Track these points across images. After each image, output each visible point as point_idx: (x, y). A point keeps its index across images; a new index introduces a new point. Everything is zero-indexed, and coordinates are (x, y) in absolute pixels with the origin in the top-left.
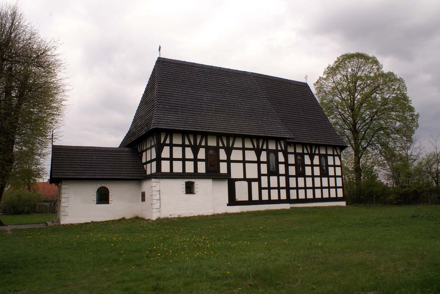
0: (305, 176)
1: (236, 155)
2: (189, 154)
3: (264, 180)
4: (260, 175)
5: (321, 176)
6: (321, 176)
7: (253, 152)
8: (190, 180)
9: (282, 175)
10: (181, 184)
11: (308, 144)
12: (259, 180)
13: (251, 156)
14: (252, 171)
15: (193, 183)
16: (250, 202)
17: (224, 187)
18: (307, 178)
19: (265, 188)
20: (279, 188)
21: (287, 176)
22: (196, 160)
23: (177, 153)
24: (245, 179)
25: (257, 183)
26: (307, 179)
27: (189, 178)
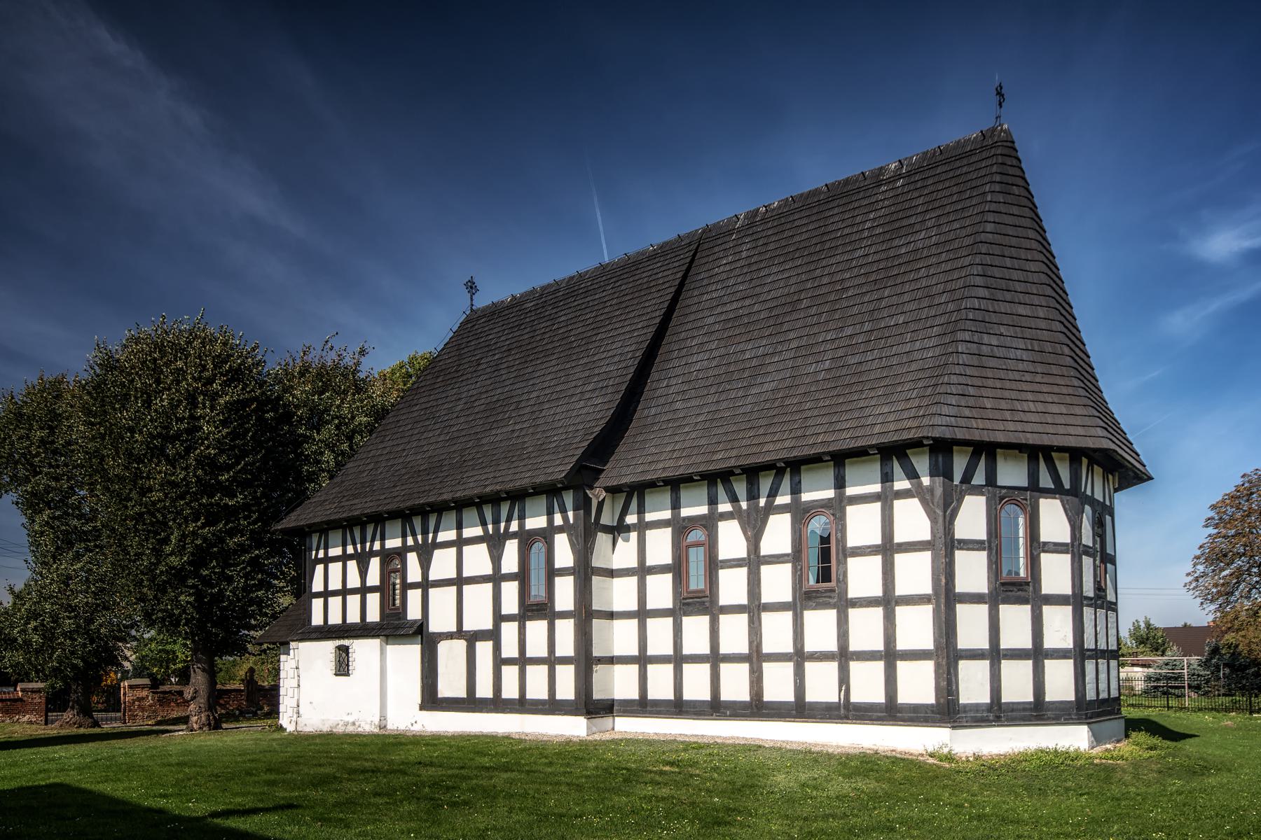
0: (844, 605)
1: (443, 565)
3: (509, 631)
4: (499, 618)
5: (804, 599)
6: (804, 599)
7: (915, 502)
9: (564, 615)
11: (917, 444)
12: (493, 635)
18: (853, 613)
19: (510, 662)
20: (552, 661)
24: (459, 633)
27: (339, 638)
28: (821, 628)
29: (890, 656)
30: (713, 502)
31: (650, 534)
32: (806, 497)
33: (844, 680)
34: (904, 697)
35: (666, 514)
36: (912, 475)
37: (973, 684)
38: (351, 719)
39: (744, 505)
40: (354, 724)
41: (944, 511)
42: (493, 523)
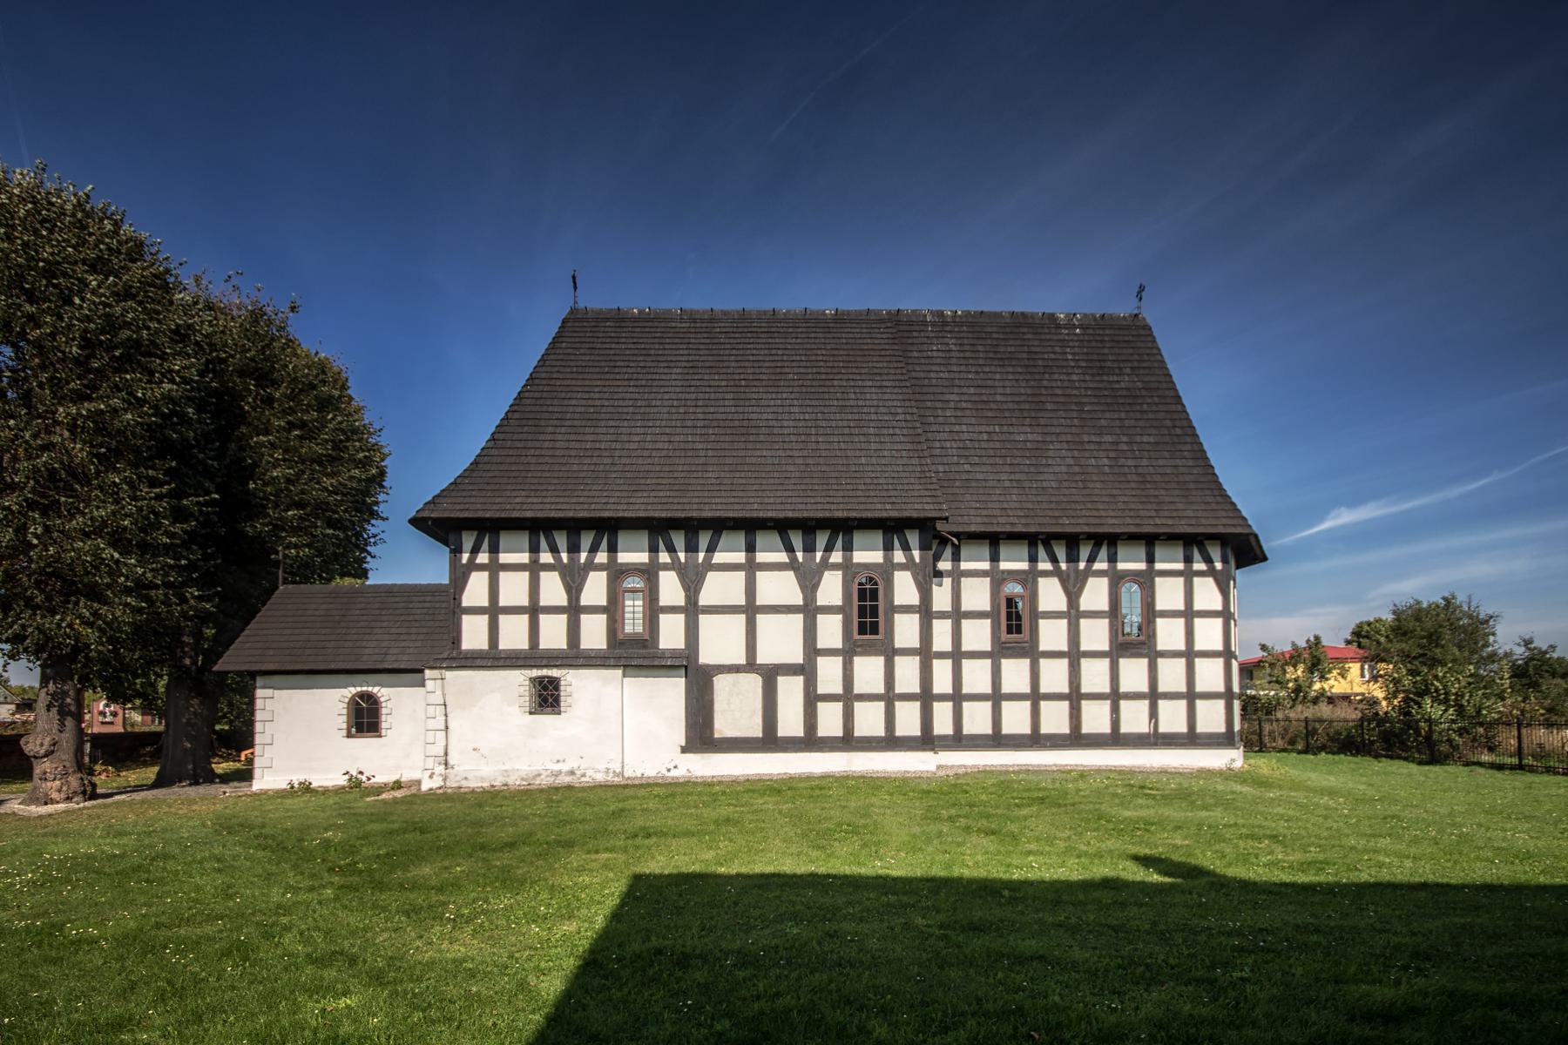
0: (1031, 652)
2: (553, 589)
4: (812, 650)
5: (998, 652)
6: (998, 652)
7: (1210, 581)
8: (545, 672)
10: (518, 681)
11: (1058, 536)
12: (807, 670)
13: (779, 587)
14: (781, 640)
15: (554, 684)
16: (770, 741)
17: (672, 691)
21: (1074, 655)
22: (574, 610)
23: (514, 589)
24: (751, 666)
25: (798, 682)
26: (899, 661)
28: (1015, 674)
29: (1191, 696)
30: (1033, 559)
31: (966, 582)
32: (1121, 566)
33: (1153, 714)
34: (1201, 728)
35: (985, 565)
36: (1208, 560)
37: (1096, 718)
38: (565, 767)
39: (564, 556)
40: (572, 773)
41: (574, 581)
42: (569, 551)
